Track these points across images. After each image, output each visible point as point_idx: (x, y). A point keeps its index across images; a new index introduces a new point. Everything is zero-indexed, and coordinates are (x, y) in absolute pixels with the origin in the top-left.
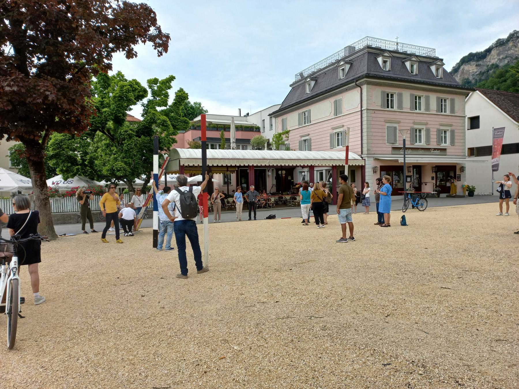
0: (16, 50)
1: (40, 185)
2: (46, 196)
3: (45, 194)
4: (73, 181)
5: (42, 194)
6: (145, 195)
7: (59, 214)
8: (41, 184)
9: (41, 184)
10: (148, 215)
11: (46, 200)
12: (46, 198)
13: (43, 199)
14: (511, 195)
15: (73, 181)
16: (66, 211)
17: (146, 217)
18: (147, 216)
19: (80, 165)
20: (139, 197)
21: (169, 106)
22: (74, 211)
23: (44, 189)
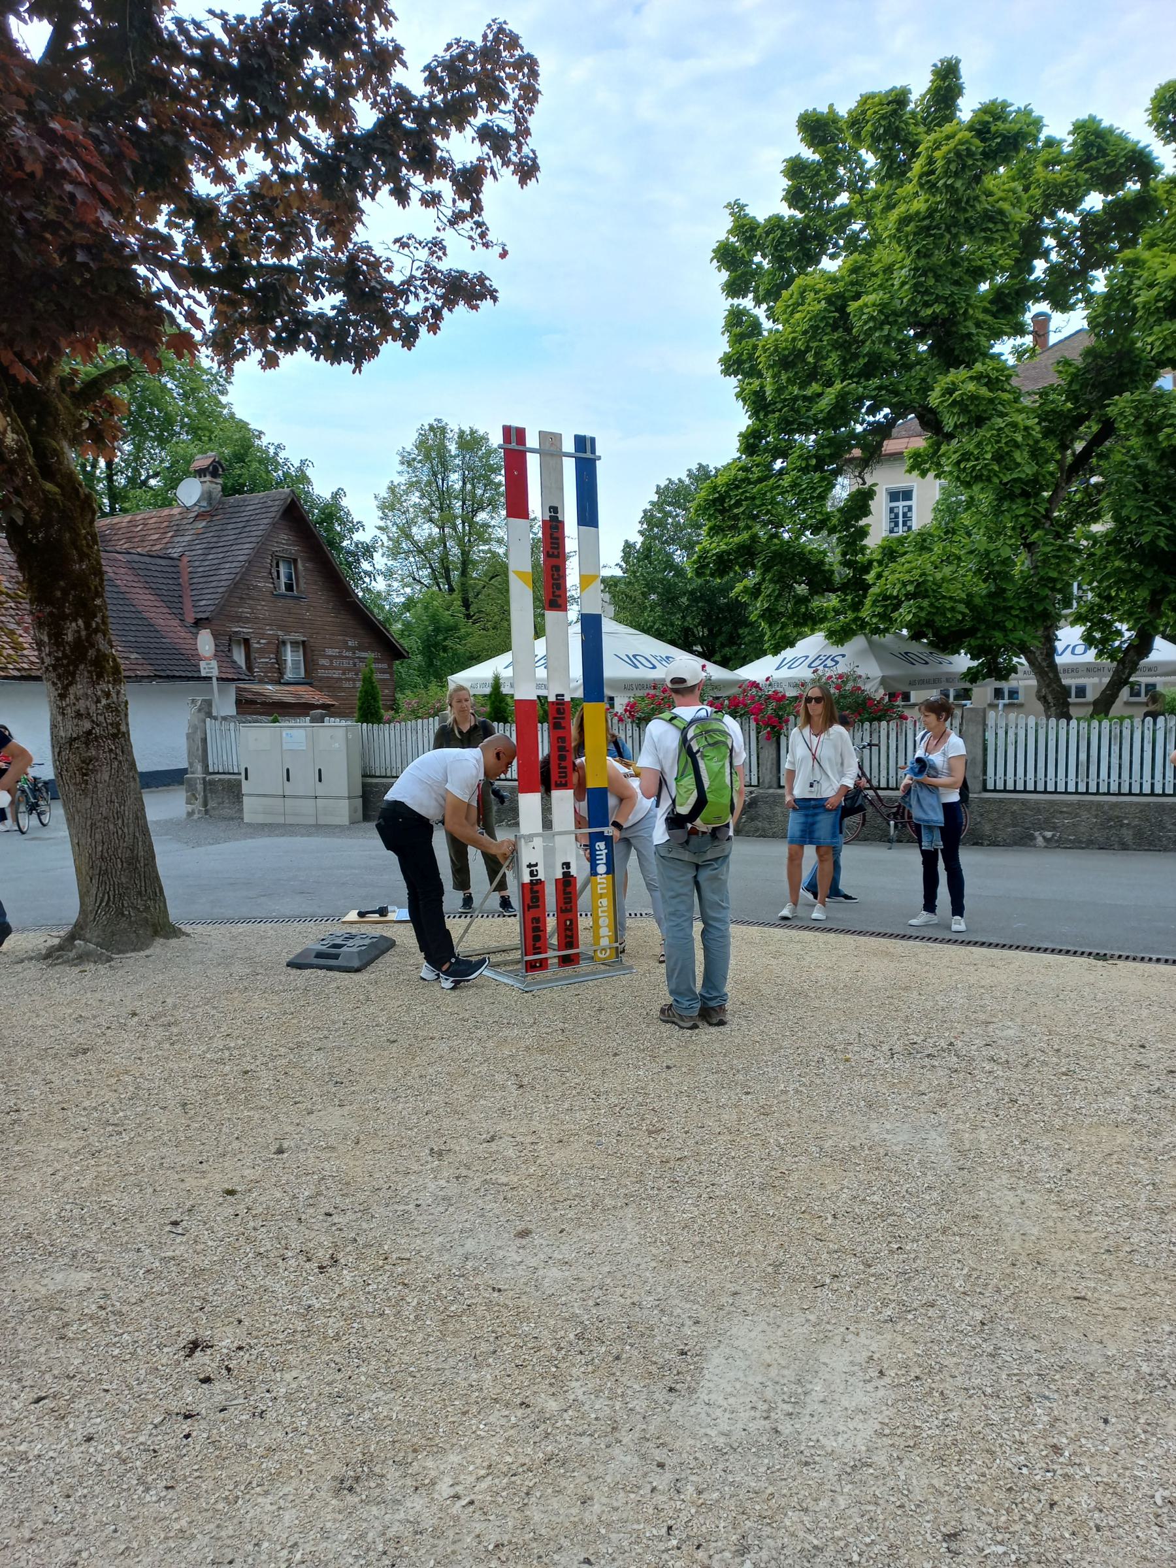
0: (370, 135)
1: (55, 667)
2: (87, 725)
3: (79, 715)
4: (844, 656)
5: (63, 714)
6: (1063, 722)
7: (1131, 804)
8: (57, 659)
9: (57, 659)
10: (1054, 828)
11: (87, 744)
12: (89, 733)
13: (72, 740)
14: (376, 831)
15: (844, 656)
16: (1020, 787)
17: (1040, 840)
18: (1049, 834)
19: (844, 588)
20: (815, 740)
21: (259, 264)
22: (1114, 788)
23: (72, 690)
